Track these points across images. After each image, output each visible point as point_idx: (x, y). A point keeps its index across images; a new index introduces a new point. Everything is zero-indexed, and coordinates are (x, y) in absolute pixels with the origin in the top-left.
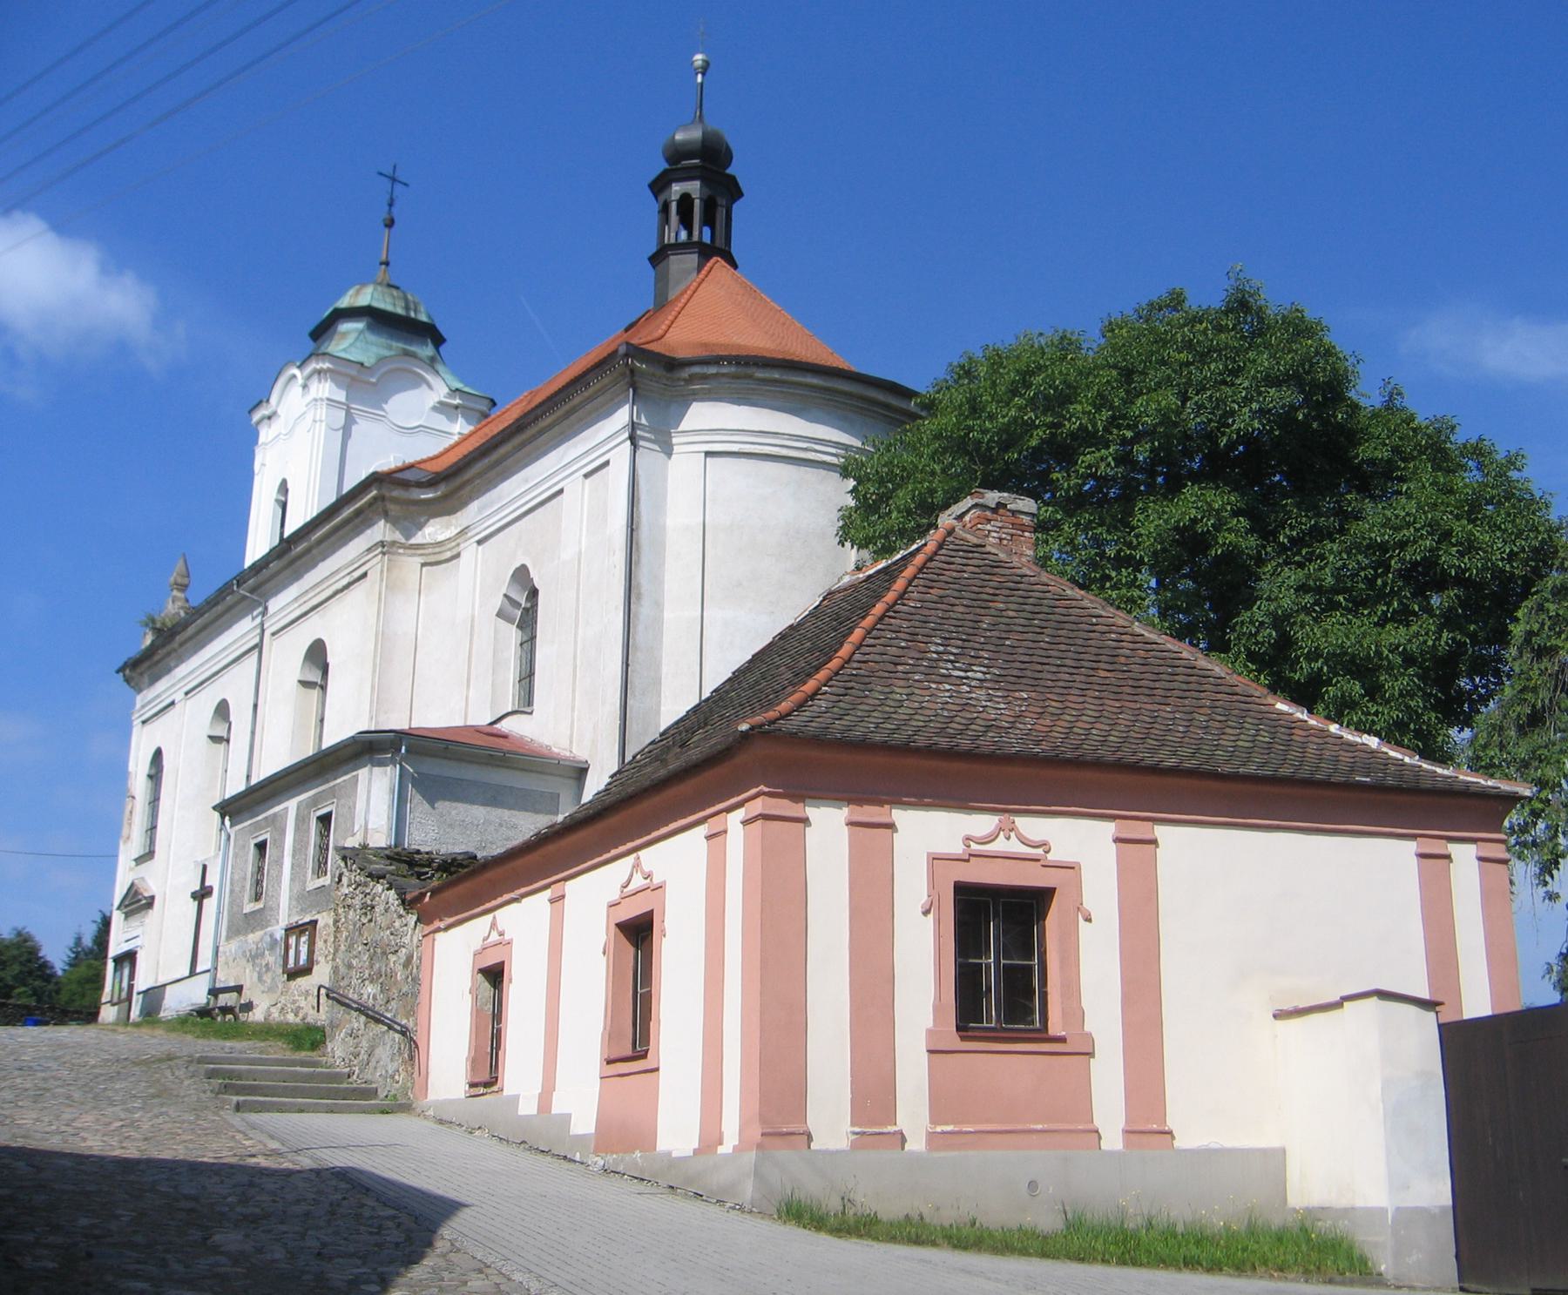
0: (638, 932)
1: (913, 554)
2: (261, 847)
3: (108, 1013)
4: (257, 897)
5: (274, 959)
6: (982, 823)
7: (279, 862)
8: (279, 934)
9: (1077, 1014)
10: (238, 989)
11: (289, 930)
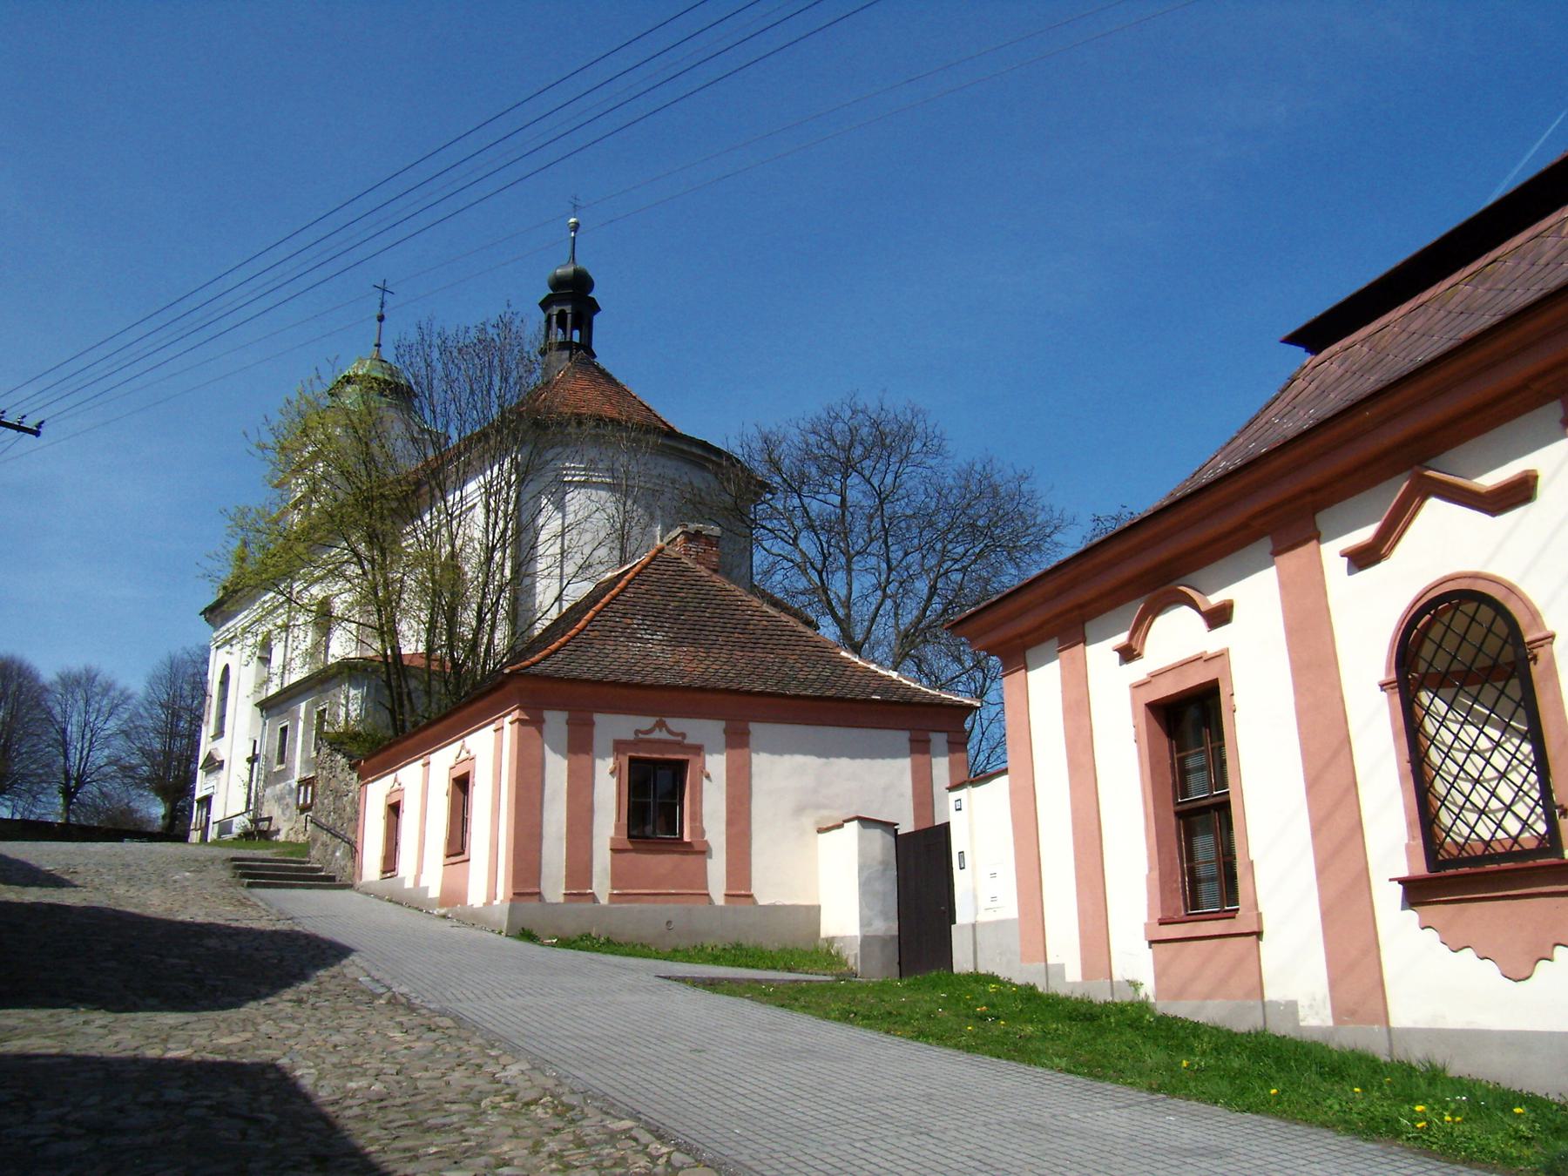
0: (462, 784)
1: (626, 572)
2: (284, 730)
3: (195, 836)
4: (281, 761)
5: (290, 800)
6: (646, 722)
7: (295, 740)
8: (294, 785)
9: (699, 831)
10: (270, 819)
11: (301, 783)
